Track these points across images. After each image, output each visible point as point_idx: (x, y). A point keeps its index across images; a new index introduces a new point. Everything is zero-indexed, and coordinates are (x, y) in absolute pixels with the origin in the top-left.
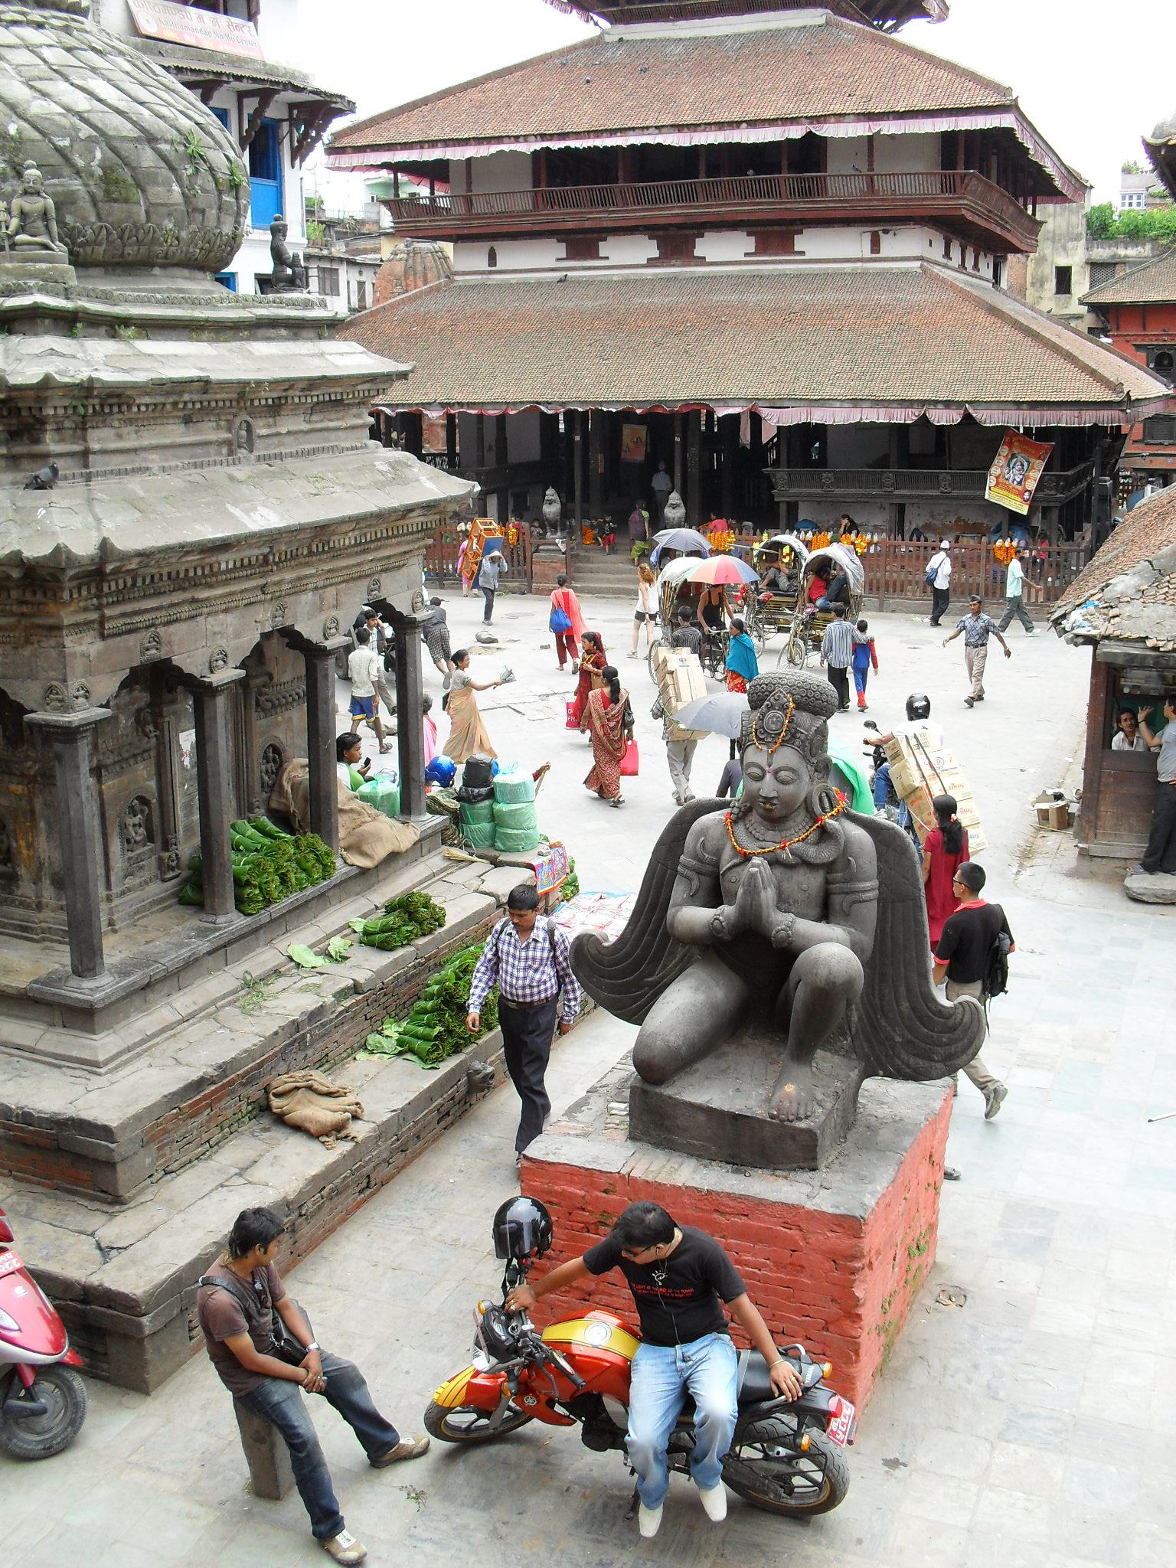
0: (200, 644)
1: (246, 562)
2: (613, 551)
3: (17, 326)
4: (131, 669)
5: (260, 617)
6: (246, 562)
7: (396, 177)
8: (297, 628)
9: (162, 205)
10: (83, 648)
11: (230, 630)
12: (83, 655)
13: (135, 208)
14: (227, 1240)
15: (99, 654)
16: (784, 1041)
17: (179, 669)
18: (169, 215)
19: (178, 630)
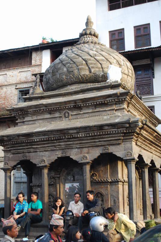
0: (38, 158)
1: (22, 141)
2: (9, 127)
3: (33, 100)
4: (20, 161)
5: (57, 153)
6: (22, 141)
7: (126, 131)
8: (71, 157)
9: (62, 73)
10: (8, 155)
11: (47, 155)
12: (8, 157)
13: (56, 76)
14: (37, 236)
15: (12, 157)
16: (110, 3)
17: (32, 162)
18: (63, 75)
19: (32, 154)
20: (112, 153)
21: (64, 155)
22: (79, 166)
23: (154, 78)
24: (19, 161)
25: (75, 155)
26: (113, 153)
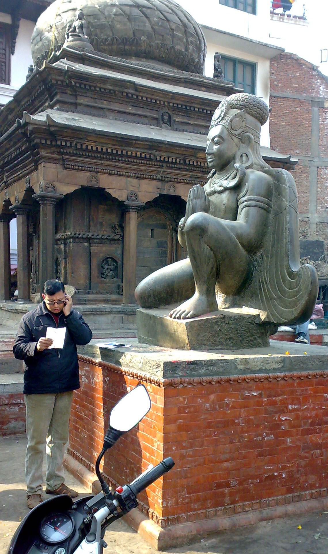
4: (82, 186)
20: (104, 189)
21: (93, 184)
22: (122, 209)
23: (13, 53)
24: (80, 187)
25: (118, 187)
26: (106, 190)
